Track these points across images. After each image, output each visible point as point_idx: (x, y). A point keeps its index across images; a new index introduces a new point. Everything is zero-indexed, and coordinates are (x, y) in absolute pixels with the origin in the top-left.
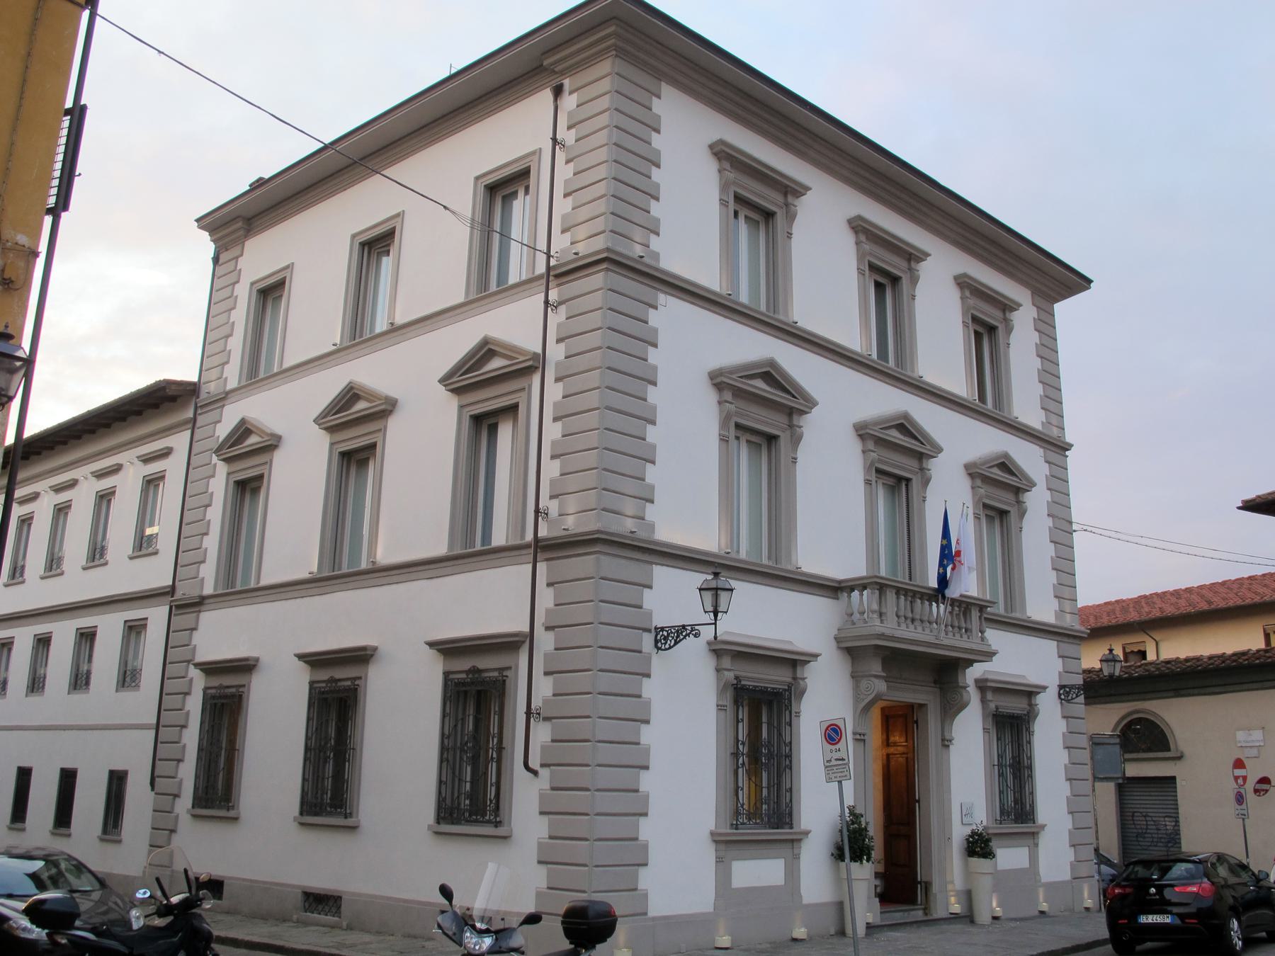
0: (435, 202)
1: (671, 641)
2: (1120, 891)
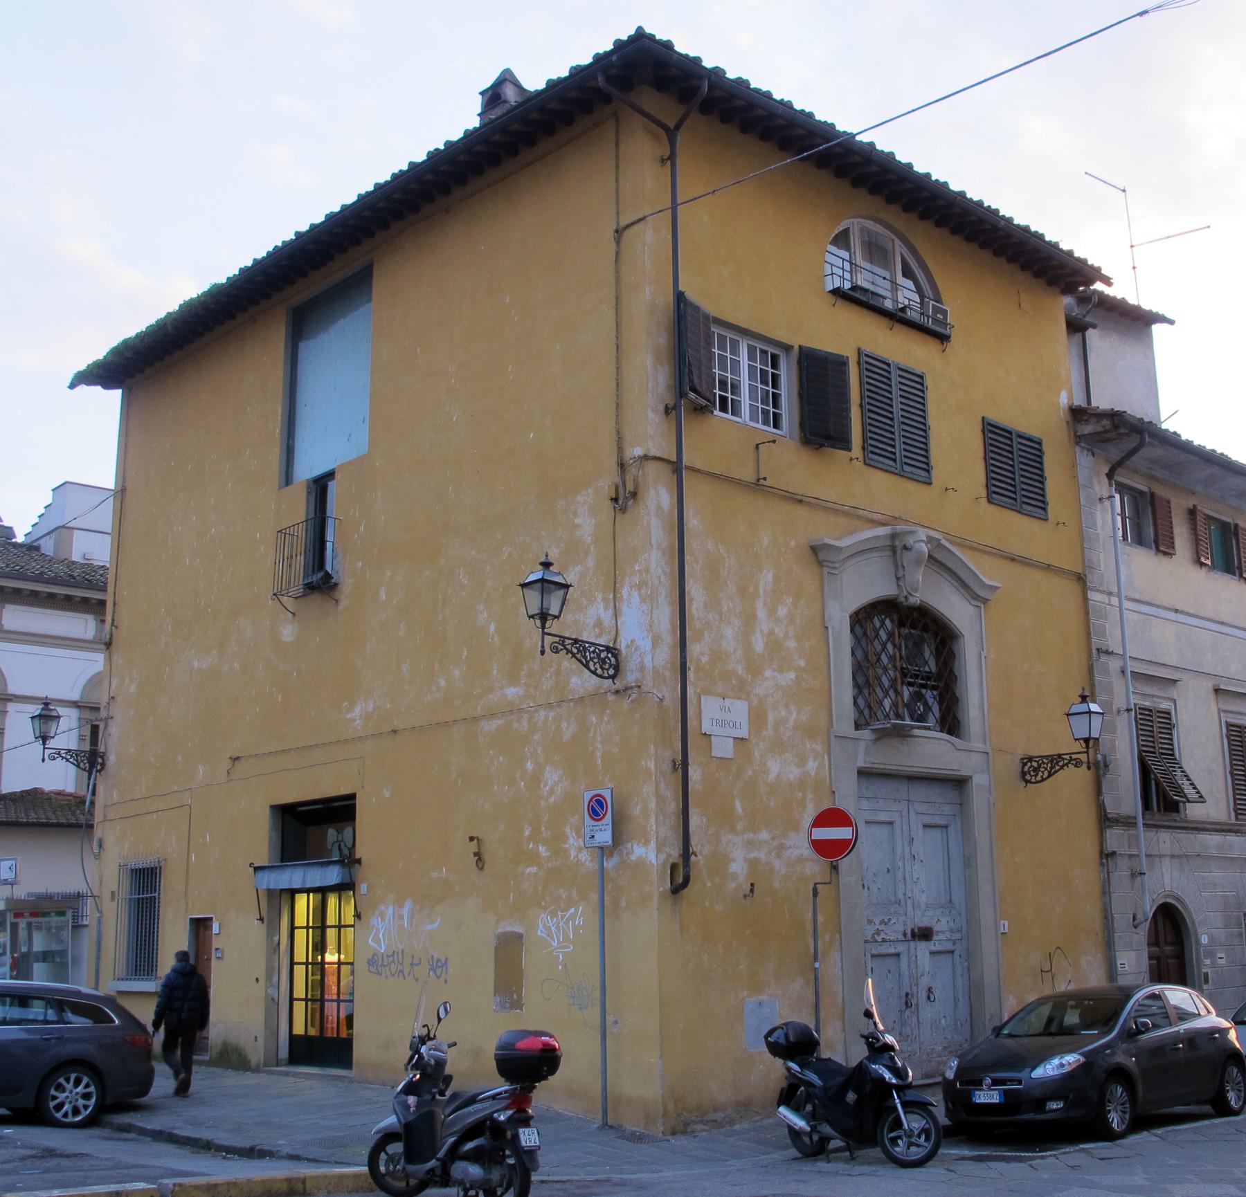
1: (1043, 772)
2: (1038, 1073)
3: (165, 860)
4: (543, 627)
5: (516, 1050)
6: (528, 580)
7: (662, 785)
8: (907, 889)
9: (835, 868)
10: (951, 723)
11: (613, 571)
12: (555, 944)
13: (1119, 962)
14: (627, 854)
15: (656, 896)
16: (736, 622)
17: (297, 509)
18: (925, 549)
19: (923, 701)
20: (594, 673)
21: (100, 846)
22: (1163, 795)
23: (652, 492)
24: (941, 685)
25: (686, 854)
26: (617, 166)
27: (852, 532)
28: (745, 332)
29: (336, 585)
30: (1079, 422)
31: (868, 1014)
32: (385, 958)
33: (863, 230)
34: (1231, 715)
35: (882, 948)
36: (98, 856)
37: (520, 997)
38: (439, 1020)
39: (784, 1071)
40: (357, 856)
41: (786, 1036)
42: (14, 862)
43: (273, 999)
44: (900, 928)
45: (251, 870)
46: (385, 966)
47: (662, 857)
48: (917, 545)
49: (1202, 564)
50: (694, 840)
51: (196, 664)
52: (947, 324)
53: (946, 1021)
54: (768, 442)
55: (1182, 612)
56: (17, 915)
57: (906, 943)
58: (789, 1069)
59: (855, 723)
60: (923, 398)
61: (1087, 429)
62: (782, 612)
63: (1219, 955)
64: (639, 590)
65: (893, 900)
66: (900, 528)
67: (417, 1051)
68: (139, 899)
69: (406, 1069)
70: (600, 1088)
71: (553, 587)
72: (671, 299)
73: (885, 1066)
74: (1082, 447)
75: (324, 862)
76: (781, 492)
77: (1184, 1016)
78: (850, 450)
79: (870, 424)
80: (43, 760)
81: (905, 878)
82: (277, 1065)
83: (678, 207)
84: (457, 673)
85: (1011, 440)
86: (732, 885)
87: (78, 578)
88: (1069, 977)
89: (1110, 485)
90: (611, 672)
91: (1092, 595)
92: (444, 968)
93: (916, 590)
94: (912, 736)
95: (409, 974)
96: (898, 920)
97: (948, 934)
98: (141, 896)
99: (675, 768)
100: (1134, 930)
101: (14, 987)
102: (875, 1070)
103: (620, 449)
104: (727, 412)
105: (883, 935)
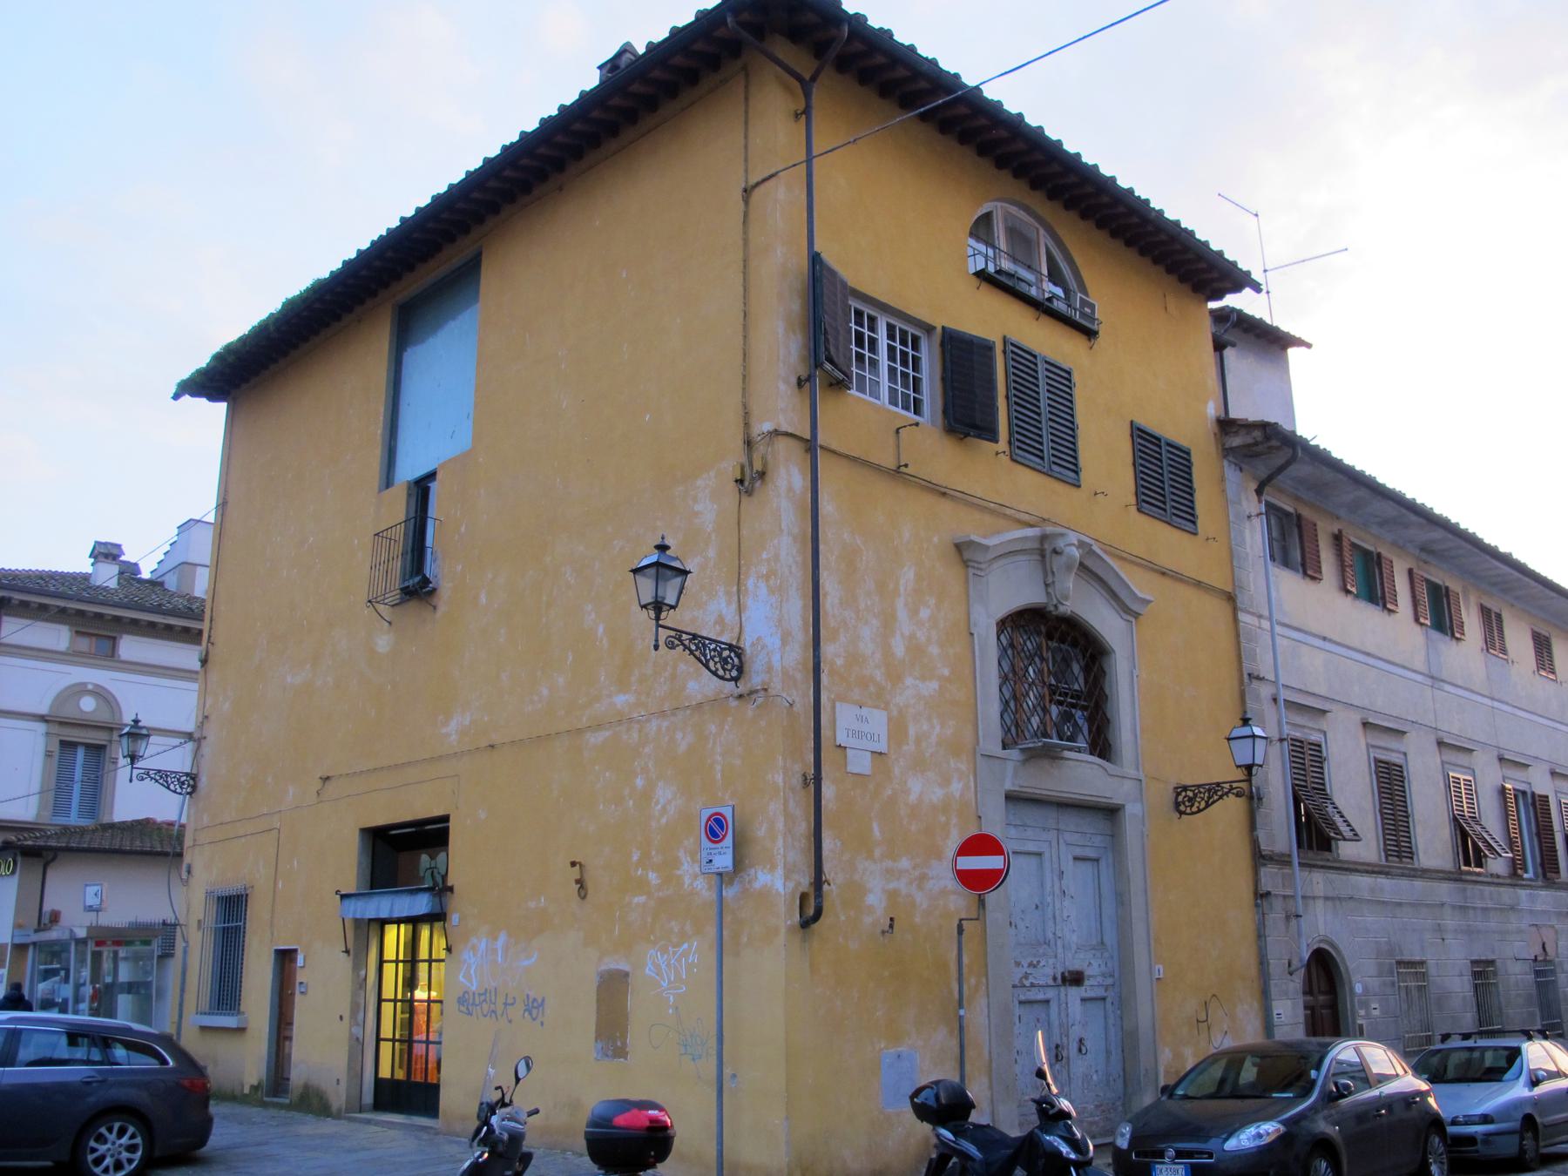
0: (1145, 10)
1: (1199, 802)
2: (1231, 1144)
3: (252, 887)
4: (658, 618)
5: (614, 1127)
6: (641, 565)
7: (791, 804)
8: (1057, 928)
9: (982, 903)
10: (1102, 746)
11: (737, 562)
12: (665, 984)
13: (1275, 1012)
14: (749, 882)
15: (783, 931)
16: (875, 622)
17: (397, 508)
18: (1076, 553)
19: (1072, 721)
20: (715, 673)
21: (189, 872)
22: (1320, 832)
23: (782, 471)
24: (1092, 705)
25: (818, 881)
26: (746, 123)
27: (998, 532)
28: (885, 308)
29: (434, 590)
30: (1226, 434)
31: (1041, 1074)
32: (477, 996)
33: (1008, 217)
34: (1378, 751)
35: (1030, 993)
36: (186, 883)
37: (624, 1044)
38: (518, 1080)
39: (934, 1141)
40: (449, 884)
41: (937, 1097)
42: (98, 888)
43: (357, 1039)
44: (1049, 971)
45: (338, 896)
46: (477, 1005)
47: (791, 885)
48: (1068, 550)
49: (1348, 592)
50: (827, 867)
51: (289, 679)
52: (1094, 319)
53: (1098, 1075)
54: (910, 425)
55: (1331, 641)
56: (98, 944)
57: (1056, 988)
58: (938, 1136)
59: (1003, 742)
60: (1071, 395)
61: (1236, 441)
62: (924, 613)
63: (1373, 1006)
64: (767, 581)
65: (1042, 940)
66: (1049, 529)
67: (486, 1122)
68: (224, 928)
69: (471, 1146)
70: (715, 1153)
71: (669, 573)
72: (804, 263)
73: (1062, 1137)
74: (1230, 461)
75: (413, 890)
76: (924, 483)
77: (1383, 1079)
78: (997, 442)
79: (1016, 418)
80: (131, 781)
81: (1054, 917)
82: (360, 1112)
83: (814, 160)
84: (561, 680)
85: (1160, 447)
86: (868, 920)
87: (196, 611)
88: (1225, 1028)
89: (1260, 502)
90: (734, 673)
91: (1242, 617)
92: (541, 1009)
93: (1067, 598)
94: (1062, 758)
95: (502, 1015)
96: (1047, 962)
97: (1100, 979)
98: (226, 925)
99: (806, 783)
100: (1289, 977)
101: (82, 1025)
102: (1049, 1142)
103: (747, 425)
104: (865, 393)
105: (1031, 980)
